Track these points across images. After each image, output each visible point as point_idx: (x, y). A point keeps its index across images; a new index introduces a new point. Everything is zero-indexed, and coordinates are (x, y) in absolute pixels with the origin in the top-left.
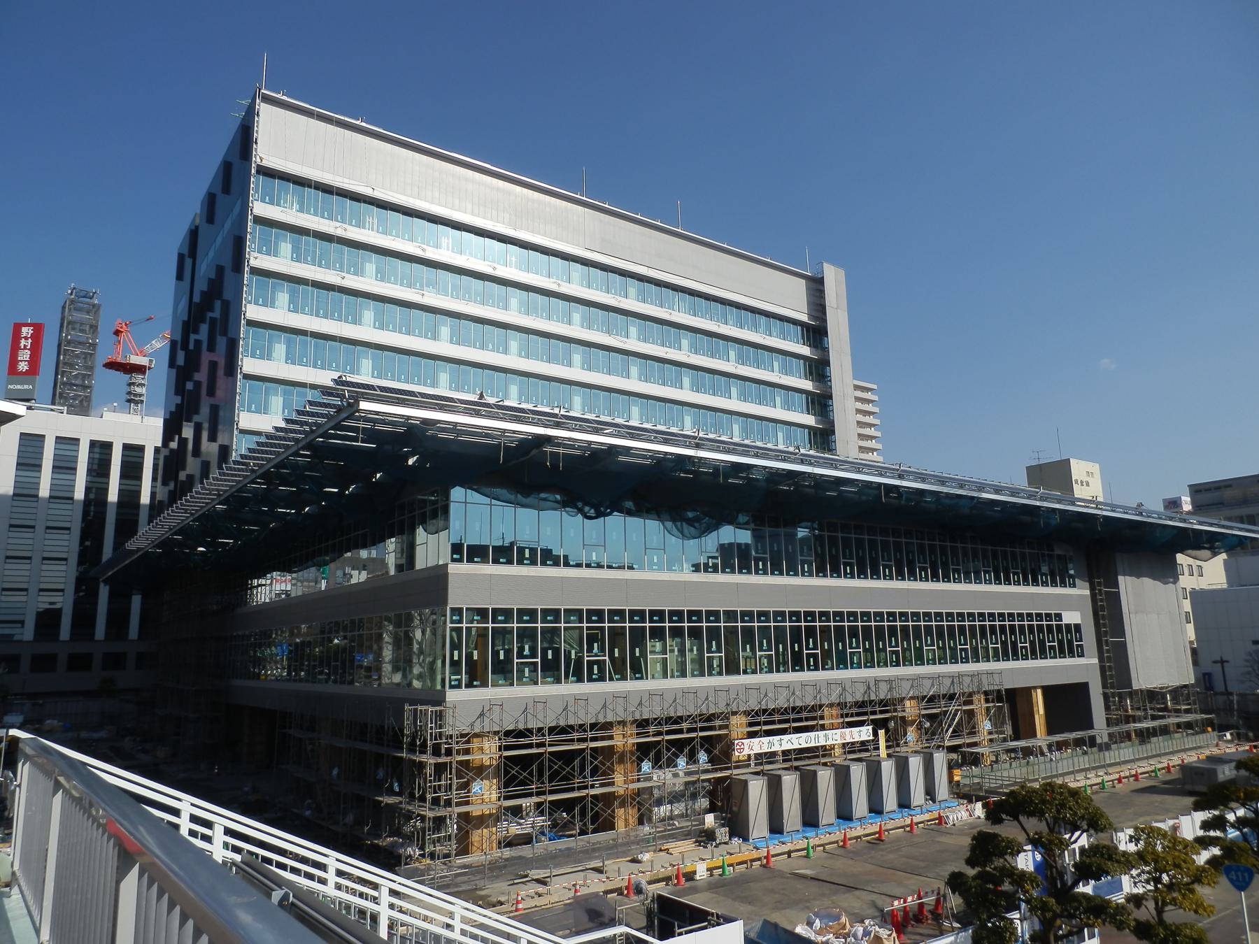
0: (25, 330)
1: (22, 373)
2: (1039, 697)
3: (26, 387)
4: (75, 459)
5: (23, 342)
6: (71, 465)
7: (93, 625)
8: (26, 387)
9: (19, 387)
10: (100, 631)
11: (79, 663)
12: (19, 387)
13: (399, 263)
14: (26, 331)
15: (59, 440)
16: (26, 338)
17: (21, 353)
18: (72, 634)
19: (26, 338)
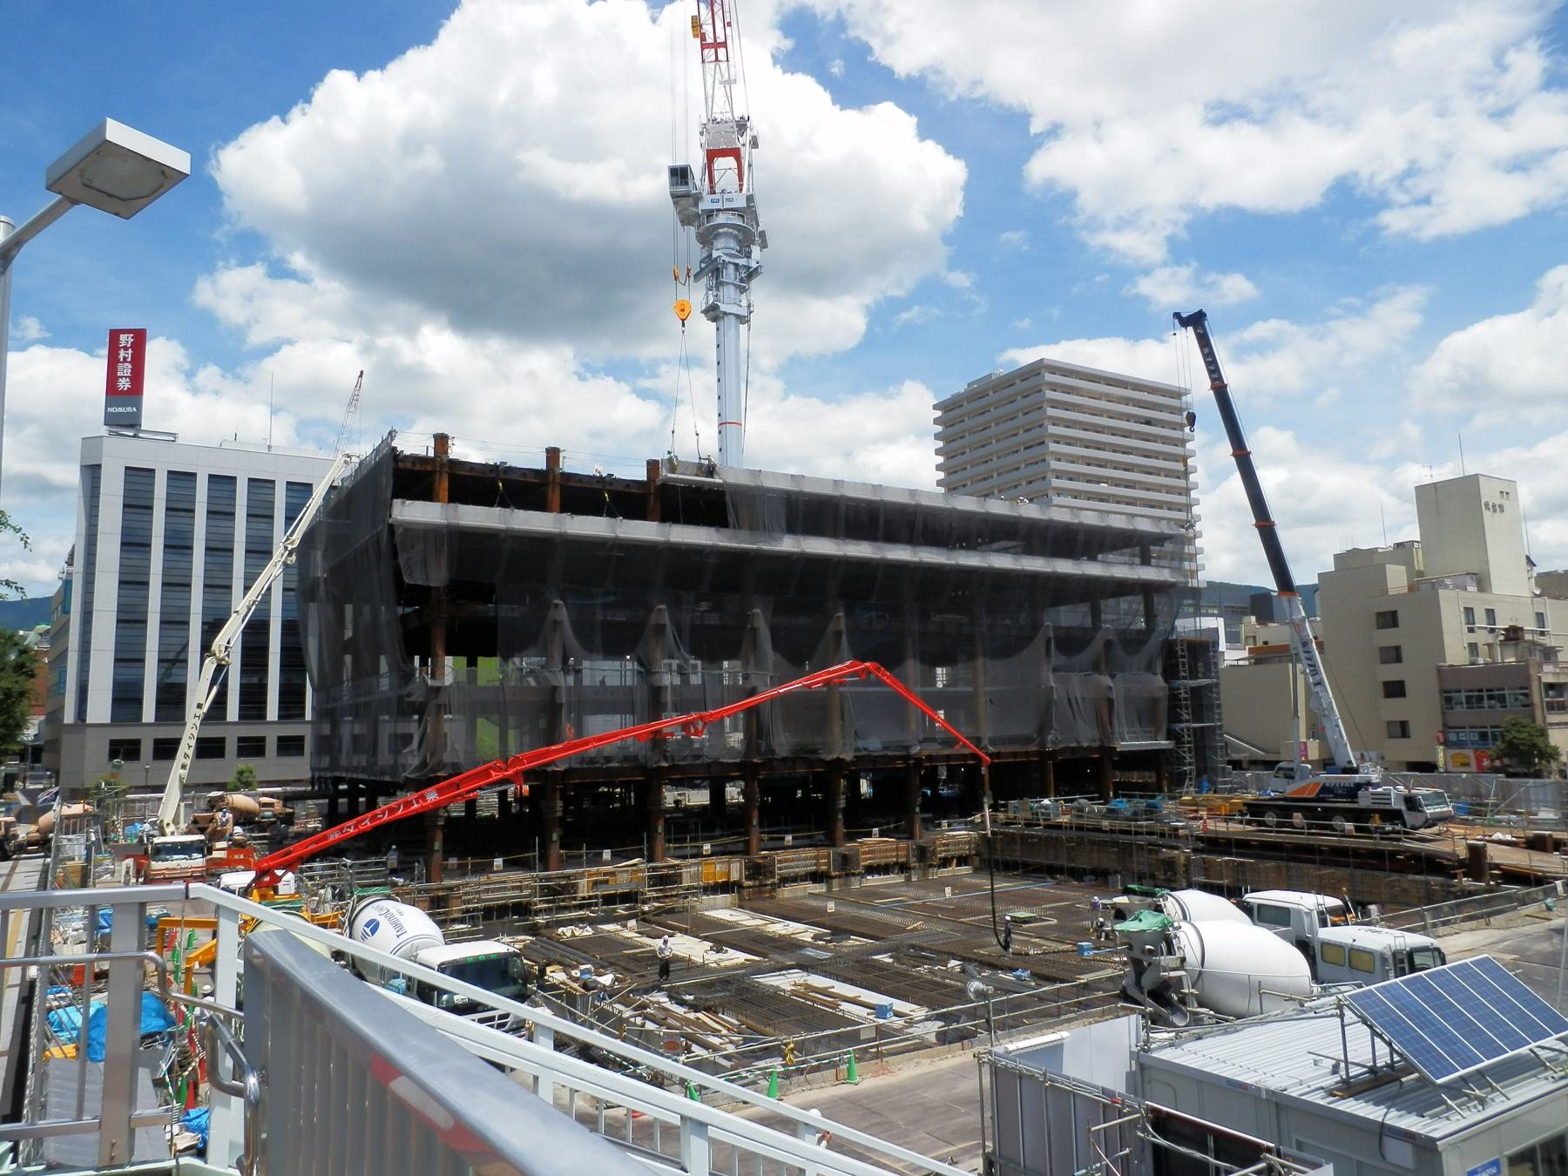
0: (123, 338)
1: (123, 393)
2: (110, 410)
3: (129, 409)
4: (271, 505)
5: (122, 353)
6: (227, 509)
7: (138, 702)
8: (129, 409)
9: (120, 410)
10: (272, 712)
11: (252, 747)
12: (120, 410)
13: (1227, 448)
14: (125, 339)
15: (172, 474)
16: (126, 348)
17: (120, 366)
18: (241, 717)
19: (126, 348)
